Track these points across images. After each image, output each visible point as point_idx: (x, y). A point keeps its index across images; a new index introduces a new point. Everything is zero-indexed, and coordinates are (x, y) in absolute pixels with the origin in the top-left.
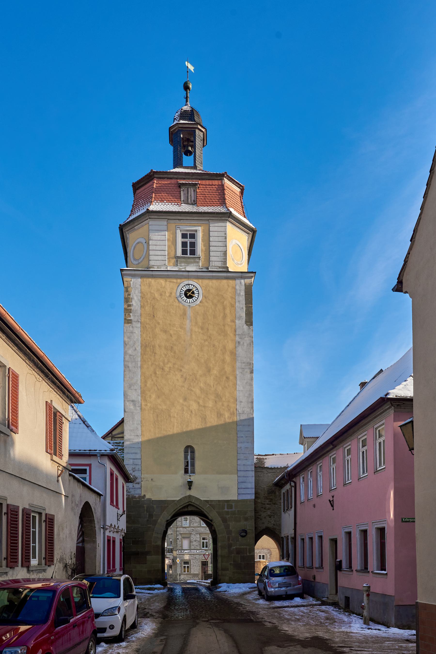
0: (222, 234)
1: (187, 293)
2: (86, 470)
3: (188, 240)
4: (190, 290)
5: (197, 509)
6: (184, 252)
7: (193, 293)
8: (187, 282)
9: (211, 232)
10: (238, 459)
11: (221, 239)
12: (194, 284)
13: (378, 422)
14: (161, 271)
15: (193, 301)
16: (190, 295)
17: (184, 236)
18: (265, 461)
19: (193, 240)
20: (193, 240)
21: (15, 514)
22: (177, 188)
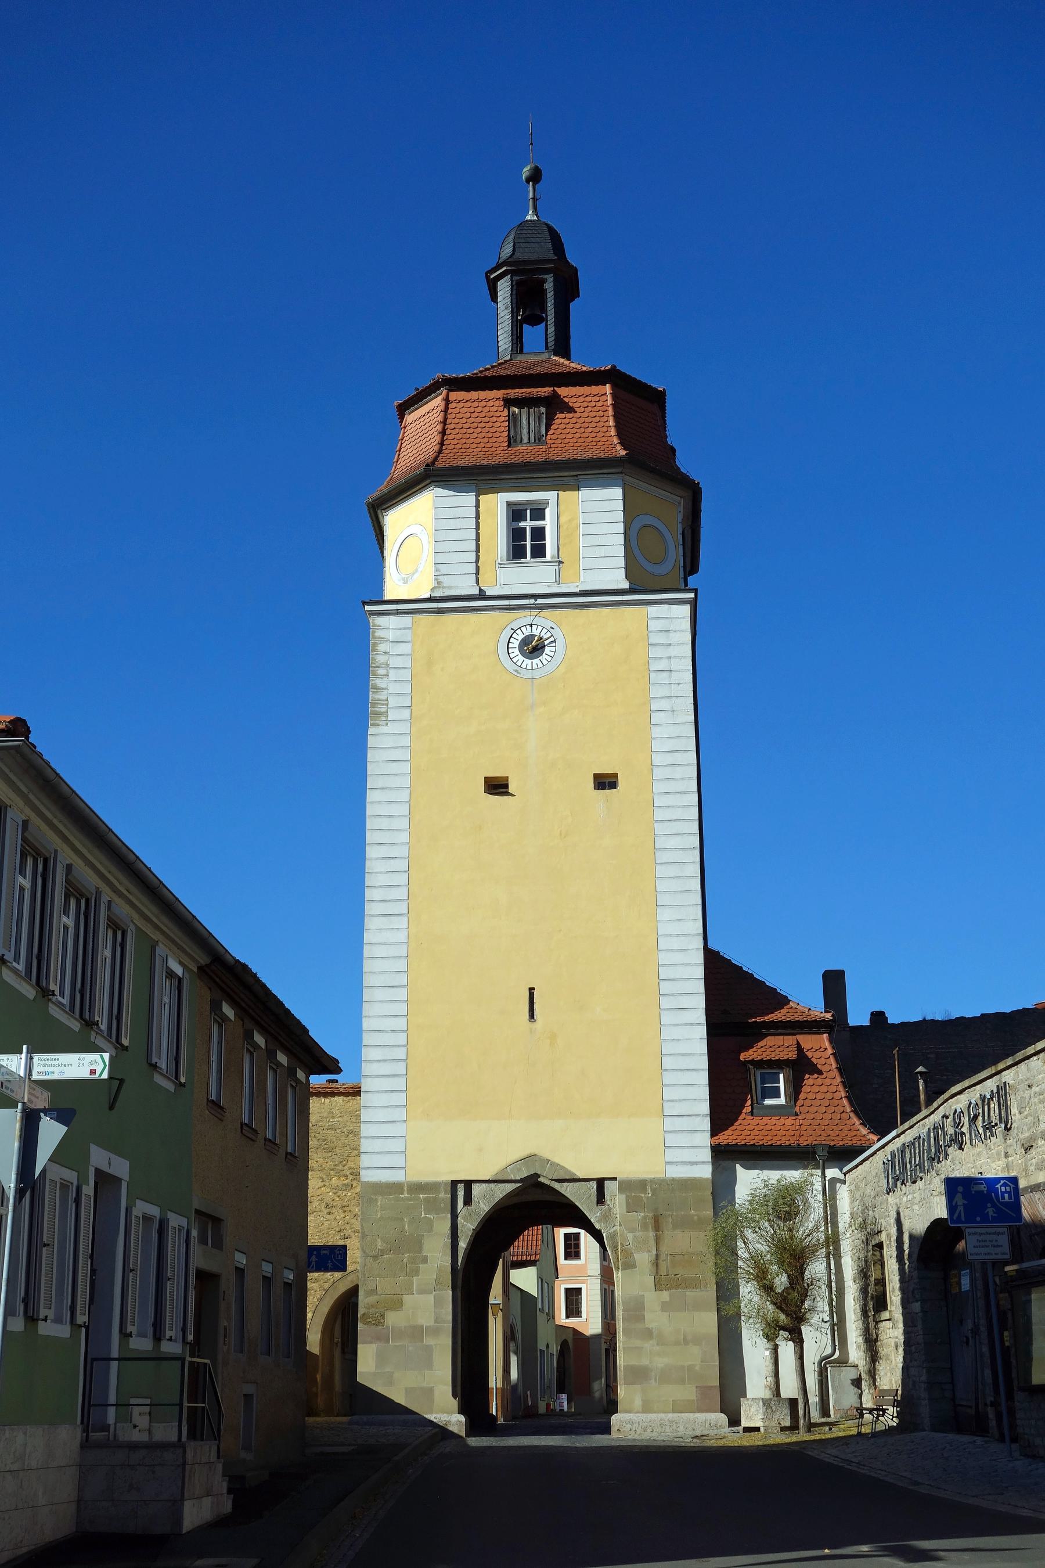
2: (567, 1236)
6: (517, 553)
8: (528, 621)
10: (666, 1070)
12: (541, 624)
15: (540, 665)
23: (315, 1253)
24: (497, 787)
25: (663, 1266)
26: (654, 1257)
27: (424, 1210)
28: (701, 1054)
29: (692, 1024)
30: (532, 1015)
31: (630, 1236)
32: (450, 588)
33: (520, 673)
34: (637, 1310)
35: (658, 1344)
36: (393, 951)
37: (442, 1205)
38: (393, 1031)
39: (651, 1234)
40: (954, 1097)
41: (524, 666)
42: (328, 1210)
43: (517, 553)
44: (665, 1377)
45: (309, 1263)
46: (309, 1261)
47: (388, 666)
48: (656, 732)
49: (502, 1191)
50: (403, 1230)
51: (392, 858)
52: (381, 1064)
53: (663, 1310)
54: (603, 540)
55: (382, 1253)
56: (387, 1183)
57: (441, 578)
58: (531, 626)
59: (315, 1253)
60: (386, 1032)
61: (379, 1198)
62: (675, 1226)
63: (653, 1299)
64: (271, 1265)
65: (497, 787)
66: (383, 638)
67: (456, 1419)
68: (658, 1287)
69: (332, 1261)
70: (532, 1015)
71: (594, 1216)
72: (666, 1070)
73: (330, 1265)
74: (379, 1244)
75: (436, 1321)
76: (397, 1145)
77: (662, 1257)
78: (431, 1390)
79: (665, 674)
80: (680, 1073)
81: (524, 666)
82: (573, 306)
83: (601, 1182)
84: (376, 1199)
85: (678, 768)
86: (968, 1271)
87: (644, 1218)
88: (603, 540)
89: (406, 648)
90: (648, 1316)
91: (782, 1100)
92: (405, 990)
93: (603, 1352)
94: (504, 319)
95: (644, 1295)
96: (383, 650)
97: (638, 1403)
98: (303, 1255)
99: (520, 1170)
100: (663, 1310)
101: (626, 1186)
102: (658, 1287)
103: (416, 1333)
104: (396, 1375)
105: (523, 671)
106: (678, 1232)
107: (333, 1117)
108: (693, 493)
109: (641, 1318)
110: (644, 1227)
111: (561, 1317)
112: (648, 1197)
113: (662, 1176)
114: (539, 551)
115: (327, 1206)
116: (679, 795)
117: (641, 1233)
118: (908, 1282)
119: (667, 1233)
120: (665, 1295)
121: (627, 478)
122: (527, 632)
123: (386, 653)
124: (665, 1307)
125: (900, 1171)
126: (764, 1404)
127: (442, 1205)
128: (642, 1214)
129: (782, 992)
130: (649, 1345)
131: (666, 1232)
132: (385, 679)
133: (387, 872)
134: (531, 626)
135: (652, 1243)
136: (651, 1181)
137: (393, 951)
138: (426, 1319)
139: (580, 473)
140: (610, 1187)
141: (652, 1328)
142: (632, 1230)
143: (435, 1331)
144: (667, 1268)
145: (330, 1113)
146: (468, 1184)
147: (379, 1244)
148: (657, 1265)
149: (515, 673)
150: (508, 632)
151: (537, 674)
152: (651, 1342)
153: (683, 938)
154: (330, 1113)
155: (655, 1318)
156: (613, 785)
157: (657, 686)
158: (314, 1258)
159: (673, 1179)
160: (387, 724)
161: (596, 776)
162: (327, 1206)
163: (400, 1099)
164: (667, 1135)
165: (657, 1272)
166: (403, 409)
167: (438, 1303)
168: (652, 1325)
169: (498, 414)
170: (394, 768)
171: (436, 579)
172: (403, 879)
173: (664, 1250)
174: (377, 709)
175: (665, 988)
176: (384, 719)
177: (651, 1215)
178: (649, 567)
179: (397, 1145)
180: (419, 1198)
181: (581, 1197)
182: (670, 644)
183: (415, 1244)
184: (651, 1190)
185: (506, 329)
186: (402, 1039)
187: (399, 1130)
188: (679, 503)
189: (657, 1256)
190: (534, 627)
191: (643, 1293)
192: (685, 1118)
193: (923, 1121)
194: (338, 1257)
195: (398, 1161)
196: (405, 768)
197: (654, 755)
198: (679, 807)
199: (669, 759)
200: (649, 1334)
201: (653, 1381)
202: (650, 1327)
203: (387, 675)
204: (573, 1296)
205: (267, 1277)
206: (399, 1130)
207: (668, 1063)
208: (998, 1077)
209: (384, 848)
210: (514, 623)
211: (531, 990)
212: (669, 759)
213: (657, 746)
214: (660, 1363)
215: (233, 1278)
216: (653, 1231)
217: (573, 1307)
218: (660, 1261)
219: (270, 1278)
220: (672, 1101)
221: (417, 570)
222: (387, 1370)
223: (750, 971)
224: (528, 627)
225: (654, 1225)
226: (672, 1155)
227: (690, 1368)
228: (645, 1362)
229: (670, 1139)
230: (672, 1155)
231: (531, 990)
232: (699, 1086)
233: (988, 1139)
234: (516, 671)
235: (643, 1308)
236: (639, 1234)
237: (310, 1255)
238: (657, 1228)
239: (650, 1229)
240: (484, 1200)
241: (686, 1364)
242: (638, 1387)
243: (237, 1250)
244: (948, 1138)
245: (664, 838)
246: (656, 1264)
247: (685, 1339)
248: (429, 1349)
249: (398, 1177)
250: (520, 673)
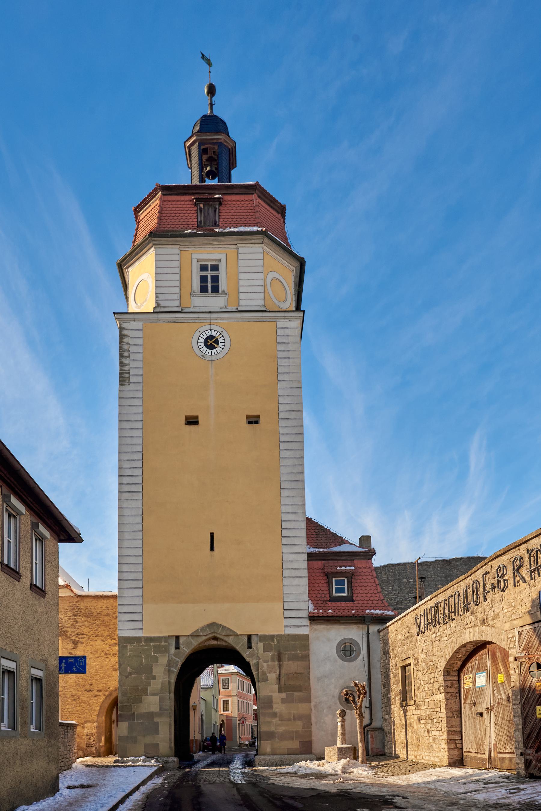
0: (126, 544)
1: (208, 340)
3: (209, 274)
4: (213, 337)
5: (226, 644)
6: (204, 289)
7: (217, 342)
8: (208, 327)
9: (239, 255)
10: (285, 577)
11: (127, 528)
13: (172, 244)
14: (277, 312)
16: (211, 344)
17: (203, 268)
18: (374, 750)
19: (214, 273)
20: (214, 273)
21: (284, 263)
22: (193, 206)
23: (64, 661)
24: (192, 421)
25: (283, 680)
26: (278, 675)
27: (153, 651)
28: (304, 569)
29: (299, 553)
30: (212, 548)
32: (164, 307)
33: (204, 357)
34: (269, 702)
35: (279, 720)
36: (134, 512)
37: (163, 649)
38: (135, 556)
39: (276, 663)
41: (207, 353)
42: (107, 656)
43: (204, 289)
44: (283, 737)
45: (60, 668)
46: (59, 666)
47: (129, 351)
48: (281, 392)
49: (195, 643)
50: (141, 662)
51: (133, 460)
52: (129, 573)
53: (282, 703)
54: (250, 289)
55: (130, 674)
57: (159, 302)
58: (211, 330)
59: (64, 661)
60: (131, 556)
61: (129, 645)
62: (289, 660)
63: (277, 697)
64: (15, 663)
65: (192, 421)
66: (127, 335)
68: (280, 691)
69: (76, 667)
70: (212, 548)
71: (246, 654)
72: (285, 577)
73: (74, 669)
74: (129, 669)
75: (160, 710)
76: (138, 617)
77: (282, 675)
78: (158, 745)
79: (286, 360)
80: (292, 579)
81: (207, 353)
82: (233, 172)
83: (249, 637)
84: (127, 646)
85: (293, 413)
86: (485, 674)
87: (273, 655)
88: (250, 289)
89: (140, 341)
90: (275, 706)
91: (346, 595)
92: (141, 533)
93: (238, 724)
94: (195, 179)
95: (271, 696)
96: (127, 342)
97: (269, 750)
98: (54, 663)
100: (282, 703)
101: (263, 638)
102: (280, 691)
103: (150, 715)
104: (139, 737)
105: (206, 356)
106: (290, 662)
107: (108, 610)
108: (302, 263)
109: (271, 707)
110: (273, 659)
111: (221, 711)
112: (275, 644)
114: (216, 289)
115: (106, 654)
116: (292, 428)
117: (271, 663)
118: (433, 683)
119: (285, 663)
120: (284, 695)
121: (265, 247)
122: (209, 334)
123: (128, 344)
124: (283, 701)
125: (432, 621)
126: (338, 750)
127: (163, 649)
128: (272, 653)
129: (345, 539)
130: (275, 721)
132: (128, 359)
133: (130, 468)
134: (211, 330)
135: (277, 668)
137: (134, 512)
138: (155, 708)
139: (239, 242)
140: (254, 639)
142: (266, 661)
143: (159, 715)
144: (285, 681)
145: (107, 607)
146: (177, 638)
147: (129, 669)
148: (279, 680)
149: (202, 357)
150: (198, 334)
151: (214, 358)
152: (276, 719)
153: (295, 506)
154: (107, 607)
155: (278, 707)
156: (256, 422)
157: (282, 367)
158: (63, 665)
159: (288, 635)
160: (129, 385)
161: (248, 417)
162: (106, 654)
163: (139, 592)
164: (285, 612)
165: (279, 683)
166: (137, 211)
167: (161, 700)
168: (277, 710)
169: (192, 209)
170: (135, 410)
171: (156, 302)
172: (139, 472)
173: (283, 672)
174: (123, 376)
175: (285, 533)
176: (127, 381)
177: (276, 653)
178: (276, 301)
179: (138, 617)
180: (151, 645)
181: (240, 647)
182: (289, 343)
183: (149, 670)
185: (196, 175)
186: (140, 560)
187: (138, 609)
188: (293, 271)
189: (280, 675)
190: (213, 331)
191: (271, 694)
192: (295, 602)
193: (459, 584)
194: (80, 664)
195: (139, 625)
196: (140, 410)
197: (280, 405)
198: (293, 434)
199: (288, 407)
200: (275, 715)
201: (277, 739)
202: (276, 711)
203: (129, 357)
204: (226, 703)
205: (9, 672)
206: (138, 609)
207: (286, 573)
208: (525, 545)
209: (129, 454)
210: (202, 328)
211: (212, 535)
212: (288, 407)
213: (281, 400)
214: (281, 729)
217: (226, 709)
218: (281, 678)
219: (13, 673)
220: (288, 594)
221: (146, 300)
222: (134, 735)
223: (328, 528)
224: (209, 331)
226: (288, 622)
227: (296, 732)
228: (272, 729)
229: (288, 614)
230: (288, 622)
231: (212, 535)
232: (303, 586)
233: (533, 579)
234: (202, 356)
235: (272, 702)
237: (60, 663)
238: (280, 660)
240: (186, 651)
241: (295, 730)
243: (32, 667)
244: (489, 587)
245: (285, 451)
246: (279, 678)
247: (294, 717)
248: (157, 724)
249: (139, 634)
250: (204, 357)
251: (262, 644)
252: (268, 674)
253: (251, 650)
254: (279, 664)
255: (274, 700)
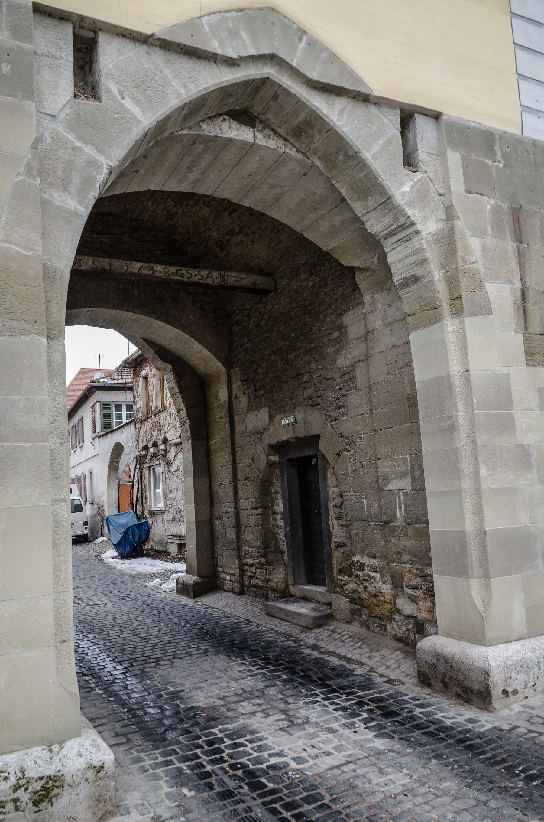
26: (519, 294)
31: (475, 243)
39: (511, 245)
40: (302, 74)
56: (322, 45)
67: (80, 764)
77: (532, 296)
87: (496, 210)
95: (508, 374)
99: (234, 34)
110: (497, 226)
113: (515, 131)
131: (533, 246)
135: (514, 264)
136: (501, 138)
141: (529, 445)
142: (479, 233)
152: (529, 476)
165: (526, 328)
177: (506, 206)
184: (503, 157)
202: (525, 442)
215: (136, 169)
216: (512, 241)
218: (529, 305)
225: (512, 227)
236: (490, 241)
239: (509, 238)
242: (516, 577)
251: (458, 156)
252: (489, 287)
253: (419, 175)
254: (518, 250)
255: (516, 394)
